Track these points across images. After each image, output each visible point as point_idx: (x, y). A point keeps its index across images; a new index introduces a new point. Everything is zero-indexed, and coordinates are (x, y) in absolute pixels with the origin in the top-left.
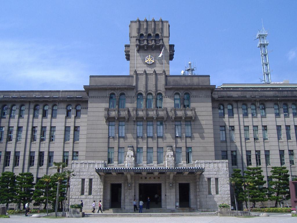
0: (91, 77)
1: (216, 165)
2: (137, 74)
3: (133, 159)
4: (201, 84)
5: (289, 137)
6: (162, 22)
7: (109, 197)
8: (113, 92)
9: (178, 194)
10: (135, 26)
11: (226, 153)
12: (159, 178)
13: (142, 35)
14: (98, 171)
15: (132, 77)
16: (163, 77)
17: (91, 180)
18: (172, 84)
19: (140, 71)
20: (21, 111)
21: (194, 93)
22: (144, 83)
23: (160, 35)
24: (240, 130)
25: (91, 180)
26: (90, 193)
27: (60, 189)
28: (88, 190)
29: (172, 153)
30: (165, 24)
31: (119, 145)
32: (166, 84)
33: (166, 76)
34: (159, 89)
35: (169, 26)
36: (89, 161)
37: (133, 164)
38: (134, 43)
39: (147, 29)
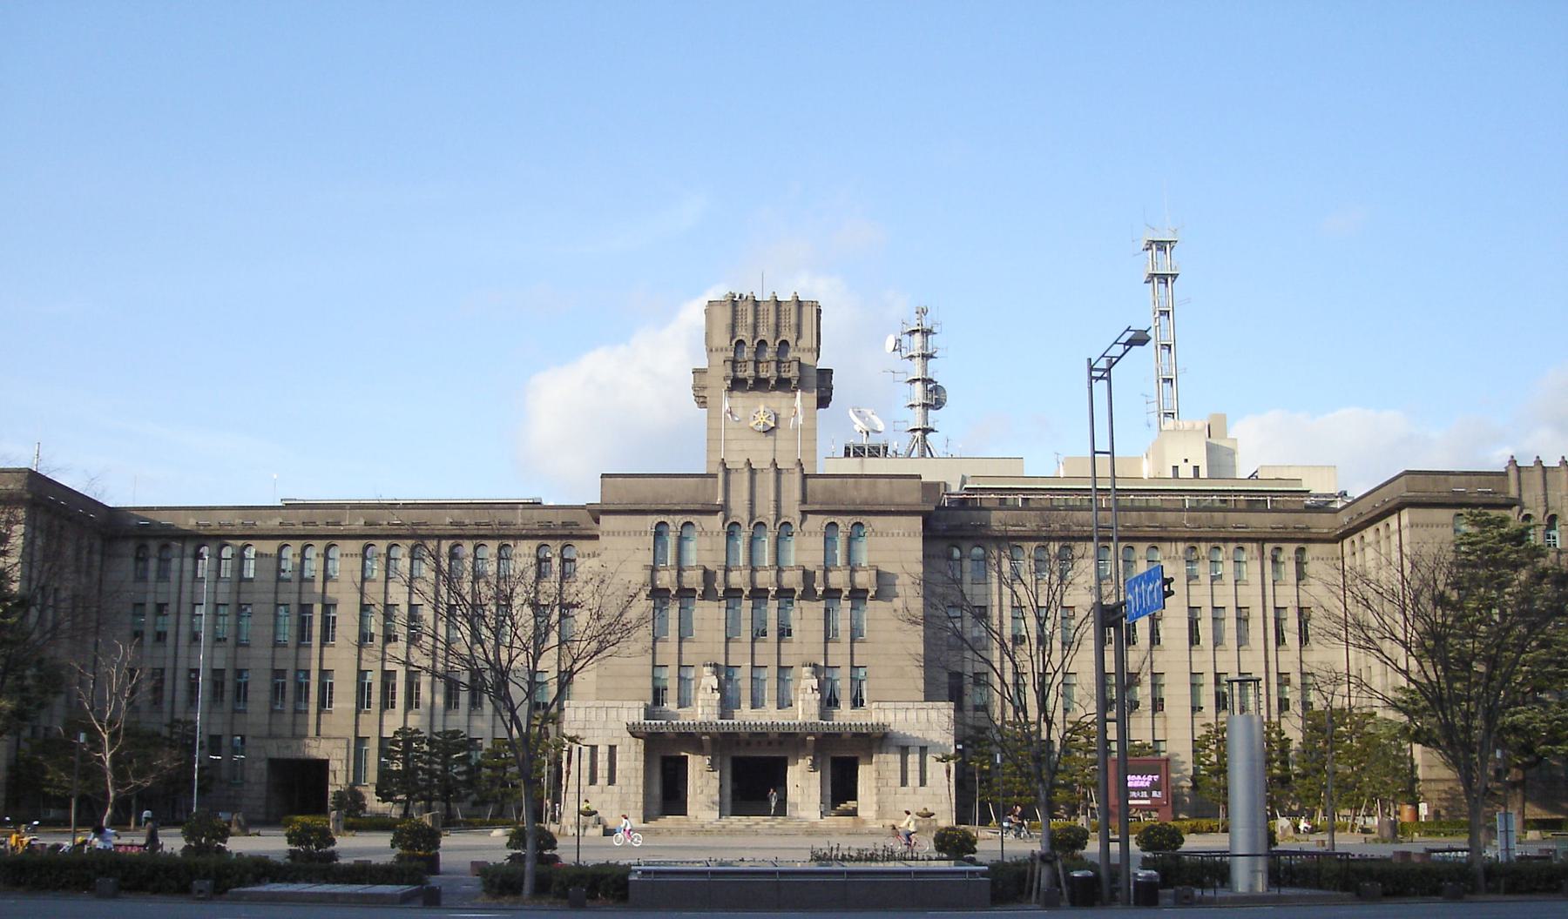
0: (603, 476)
1: (923, 714)
2: (727, 471)
3: (718, 696)
4: (897, 500)
5: (1242, 640)
6: (799, 304)
7: (657, 790)
8: (662, 518)
9: (953, 789)
10: (724, 316)
11: (949, 680)
12: (781, 743)
13: (741, 343)
14: (634, 731)
15: (715, 476)
16: (797, 477)
17: (612, 748)
18: (820, 497)
19: (736, 461)
20: (1300, 564)
21: (878, 522)
22: (746, 496)
23: (792, 343)
24: (178, 613)
25: (612, 748)
26: (612, 781)
27: (100, 721)
28: (606, 774)
29: (815, 683)
30: (806, 310)
31: (680, 660)
32: (804, 501)
33: (805, 477)
34: (784, 511)
35: (819, 311)
36: (607, 703)
37: (716, 710)
38: (722, 371)
39: (755, 327)
